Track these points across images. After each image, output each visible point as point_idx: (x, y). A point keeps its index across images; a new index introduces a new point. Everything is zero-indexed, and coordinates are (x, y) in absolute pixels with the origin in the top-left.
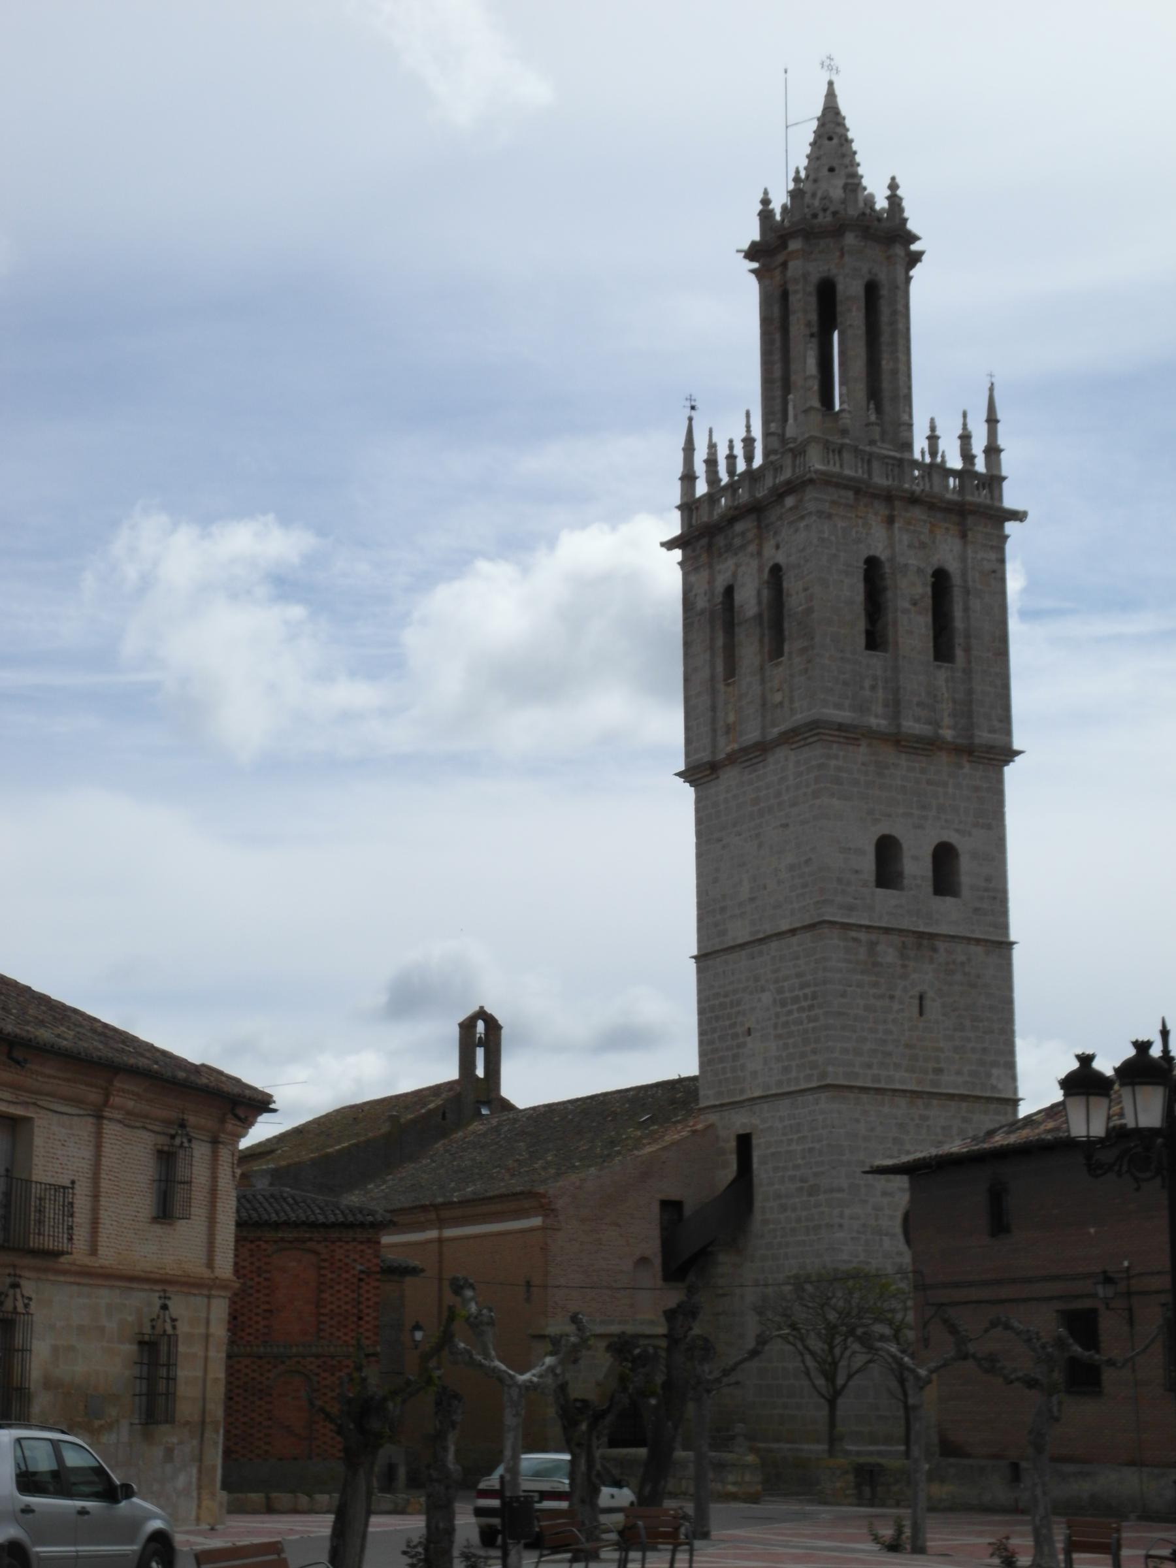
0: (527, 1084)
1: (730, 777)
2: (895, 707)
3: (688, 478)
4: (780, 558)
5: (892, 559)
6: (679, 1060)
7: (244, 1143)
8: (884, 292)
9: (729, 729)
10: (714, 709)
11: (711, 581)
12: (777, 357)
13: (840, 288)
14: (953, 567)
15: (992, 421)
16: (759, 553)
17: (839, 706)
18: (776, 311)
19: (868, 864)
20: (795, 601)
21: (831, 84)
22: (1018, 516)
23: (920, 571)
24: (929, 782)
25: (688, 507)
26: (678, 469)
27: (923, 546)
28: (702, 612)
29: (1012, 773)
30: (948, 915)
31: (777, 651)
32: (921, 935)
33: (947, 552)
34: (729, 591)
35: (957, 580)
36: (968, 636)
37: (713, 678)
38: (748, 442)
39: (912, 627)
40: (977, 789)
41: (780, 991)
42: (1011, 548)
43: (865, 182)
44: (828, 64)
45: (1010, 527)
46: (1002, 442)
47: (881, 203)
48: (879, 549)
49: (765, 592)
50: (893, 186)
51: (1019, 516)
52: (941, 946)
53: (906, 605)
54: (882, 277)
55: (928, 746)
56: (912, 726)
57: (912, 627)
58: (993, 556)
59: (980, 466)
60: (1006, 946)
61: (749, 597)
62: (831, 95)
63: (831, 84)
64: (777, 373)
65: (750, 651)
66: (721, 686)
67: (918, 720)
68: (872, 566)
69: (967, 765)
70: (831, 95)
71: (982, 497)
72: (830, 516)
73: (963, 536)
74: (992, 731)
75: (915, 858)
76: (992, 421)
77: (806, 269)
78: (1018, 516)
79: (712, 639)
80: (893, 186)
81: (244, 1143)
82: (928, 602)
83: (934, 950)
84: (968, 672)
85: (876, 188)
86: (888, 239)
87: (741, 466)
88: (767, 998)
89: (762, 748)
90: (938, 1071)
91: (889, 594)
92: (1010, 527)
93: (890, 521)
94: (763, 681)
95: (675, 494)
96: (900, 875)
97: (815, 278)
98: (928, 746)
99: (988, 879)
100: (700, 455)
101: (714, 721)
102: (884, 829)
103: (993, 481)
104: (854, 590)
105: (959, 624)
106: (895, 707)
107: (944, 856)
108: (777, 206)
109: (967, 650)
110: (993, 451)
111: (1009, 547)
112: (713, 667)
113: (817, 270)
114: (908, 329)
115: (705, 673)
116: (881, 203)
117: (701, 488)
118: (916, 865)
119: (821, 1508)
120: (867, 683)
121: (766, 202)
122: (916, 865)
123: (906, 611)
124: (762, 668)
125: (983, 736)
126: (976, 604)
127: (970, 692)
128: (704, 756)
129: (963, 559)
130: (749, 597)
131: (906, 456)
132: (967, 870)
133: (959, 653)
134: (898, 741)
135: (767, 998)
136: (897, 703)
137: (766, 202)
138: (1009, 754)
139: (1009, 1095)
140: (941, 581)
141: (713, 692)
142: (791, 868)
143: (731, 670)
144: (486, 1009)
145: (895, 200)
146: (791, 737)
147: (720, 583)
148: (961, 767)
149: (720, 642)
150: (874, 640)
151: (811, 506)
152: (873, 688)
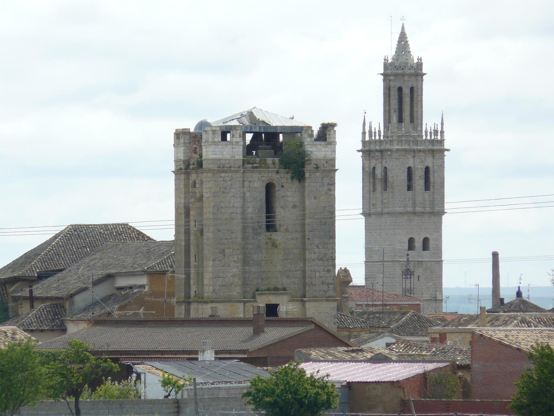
2: (414, 205)
3: (364, 133)
4: (387, 166)
5: (414, 166)
6: (364, 284)
8: (415, 89)
9: (373, 205)
10: (370, 198)
11: (370, 164)
12: (387, 104)
13: (404, 90)
14: (430, 165)
15: (442, 124)
16: (382, 163)
17: (400, 207)
18: (387, 92)
20: (390, 179)
21: (403, 24)
23: (421, 168)
24: (423, 222)
25: (364, 142)
27: (423, 161)
28: (367, 172)
30: (426, 256)
31: (385, 188)
32: (419, 261)
33: (429, 162)
34: (374, 168)
35: (431, 169)
36: (434, 183)
37: (370, 190)
38: (379, 131)
39: (419, 183)
40: (435, 222)
42: (446, 159)
43: (412, 53)
44: (403, 18)
45: (446, 153)
46: (444, 129)
48: (411, 165)
49: (383, 173)
50: (403, 85)
51: (448, 150)
52: (424, 263)
53: (418, 178)
54: (415, 85)
55: (422, 213)
56: (418, 209)
57: (419, 183)
58: (441, 161)
61: (379, 172)
62: (403, 28)
63: (403, 24)
64: (387, 109)
65: (379, 187)
66: (372, 193)
67: (420, 207)
68: (409, 169)
69: (432, 218)
70: (403, 28)
72: (399, 159)
73: (433, 157)
74: (439, 207)
75: (418, 242)
76: (442, 124)
77: (395, 84)
79: (370, 180)
82: (424, 176)
83: (422, 264)
84: (433, 193)
86: (416, 73)
87: (377, 138)
89: (382, 214)
90: (422, 294)
91: (413, 176)
92: (446, 153)
93: (414, 157)
94: (382, 196)
95: (360, 138)
96: (414, 246)
97: (397, 87)
98: (422, 213)
99: (437, 245)
100: (367, 129)
101: (370, 202)
102: (410, 236)
103: (442, 142)
104: (404, 176)
105: (431, 180)
106: (414, 205)
107: (426, 241)
109: (434, 187)
111: (445, 158)
112: (370, 187)
113: (398, 85)
114: (422, 100)
115: (367, 188)
117: (367, 138)
118: (418, 244)
119: (307, 364)
120: (407, 200)
122: (418, 244)
123: (417, 180)
124: (382, 193)
125: (437, 209)
126: (436, 175)
127: (434, 198)
129: (433, 163)
130: (379, 172)
132: (431, 244)
133: (431, 188)
134: (414, 213)
136: (415, 203)
138: (444, 213)
139: (441, 298)
140: (427, 169)
141: (370, 194)
144: (259, 116)
146: (388, 213)
147: (372, 165)
148: (431, 217)
149: (372, 181)
150: (409, 188)
151: (394, 157)
152: (409, 200)
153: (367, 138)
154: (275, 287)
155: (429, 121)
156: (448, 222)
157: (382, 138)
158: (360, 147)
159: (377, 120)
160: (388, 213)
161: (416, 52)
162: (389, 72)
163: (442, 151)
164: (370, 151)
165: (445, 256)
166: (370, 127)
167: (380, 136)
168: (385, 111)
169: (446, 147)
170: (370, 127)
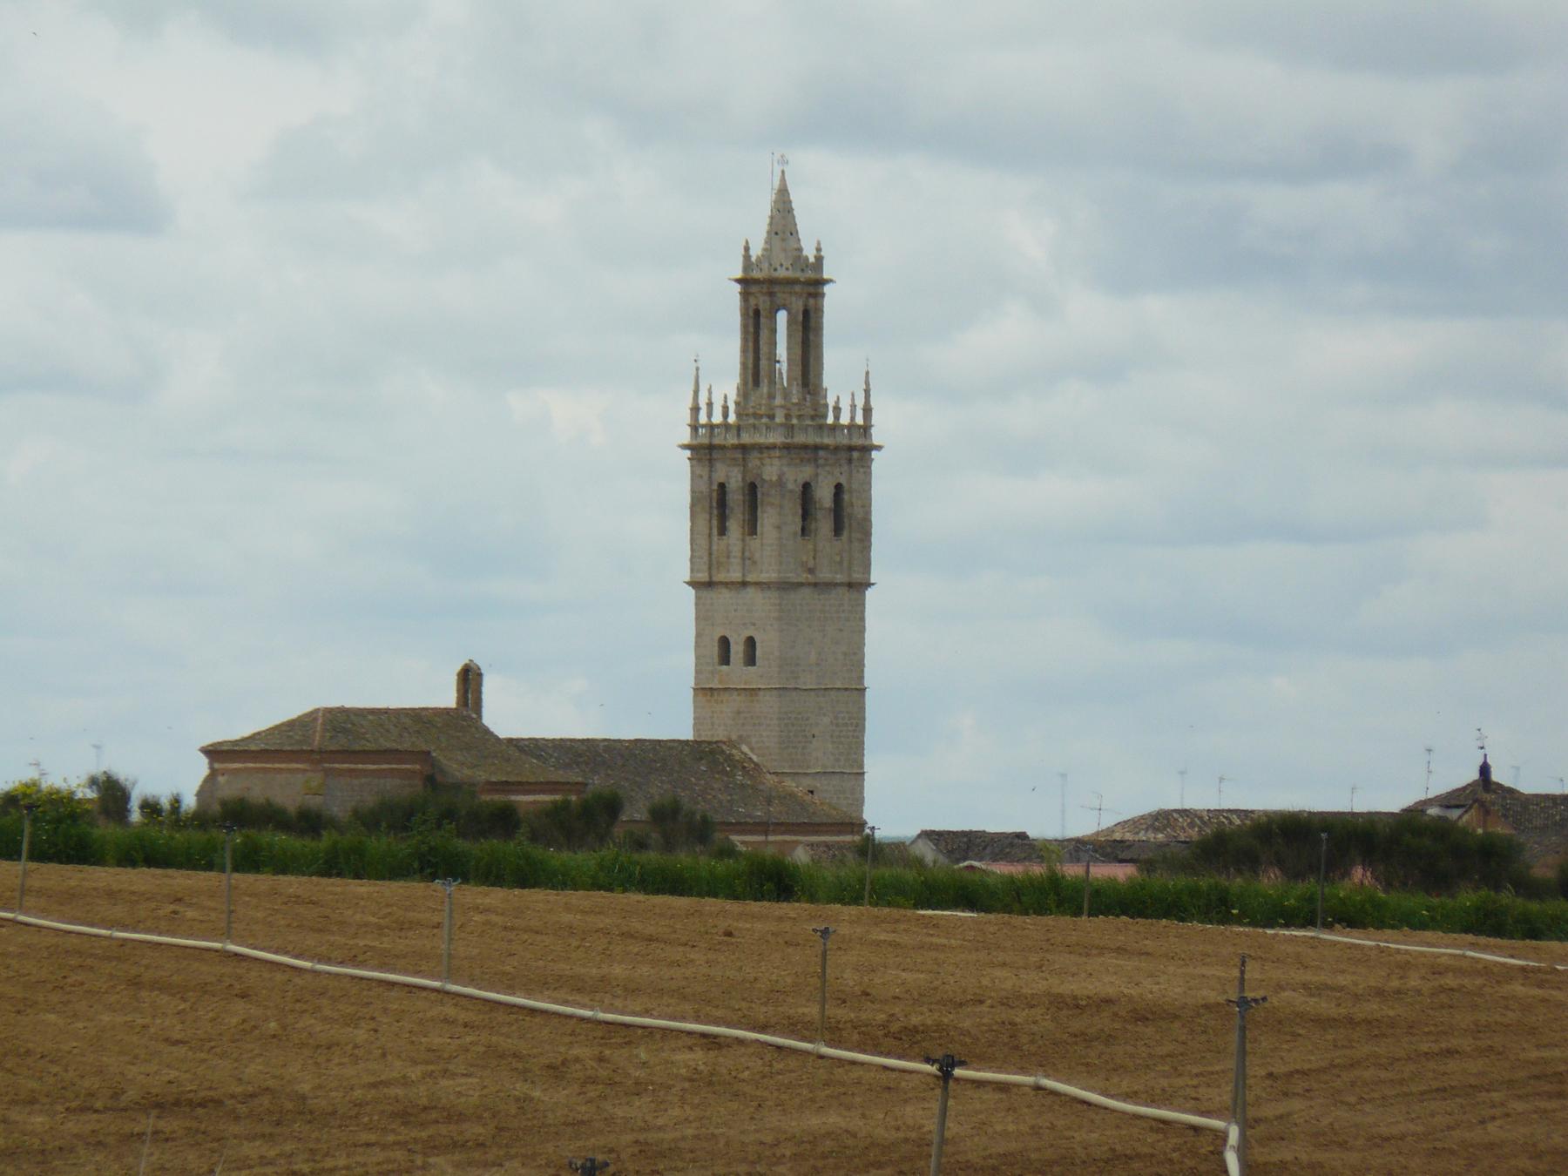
0: (985, 720)
1: (723, 597)
3: (695, 410)
15: (867, 392)
19: (715, 650)
26: (689, 403)
41: (836, 718)
46: (873, 404)
47: (812, 260)
50: (819, 250)
51: (879, 448)
59: (859, 420)
66: (715, 538)
71: (858, 441)
76: (867, 392)
80: (819, 250)
85: (809, 253)
88: (826, 720)
89: (744, 584)
95: (687, 417)
103: (866, 429)
110: (867, 411)
116: (812, 260)
118: (737, 650)
121: (747, 249)
122: (737, 650)
131: (821, 422)
132: (715, 650)
135: (826, 720)
137: (747, 249)
140: (839, 487)
142: (845, 654)
143: (723, 531)
145: (819, 259)
153: (703, 419)
157: (732, 419)
158: (685, 436)
159: (725, 387)
160: (757, 584)
162: (756, 274)
163: (867, 449)
164: (737, 404)
165: (1348, 810)
167: (726, 415)
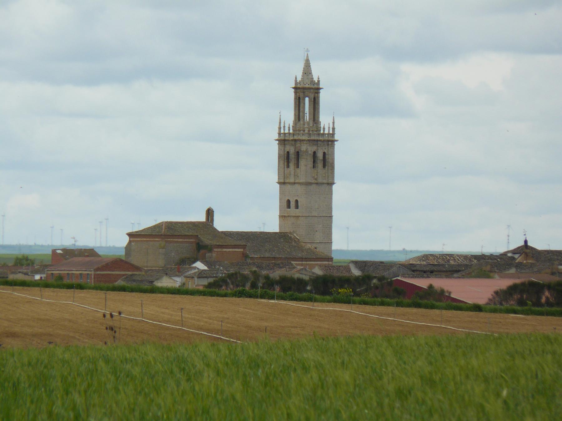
3: (280, 128)
7: (206, 268)
15: (333, 123)
22: (337, 141)
25: (280, 134)
26: (278, 126)
29: (334, 187)
47: (316, 81)
59: (331, 132)
60: (331, 217)
61: (320, 155)
66: (286, 168)
76: (333, 123)
78: (337, 141)
81: (206, 268)
85: (316, 79)
88: (321, 226)
89: (295, 183)
108: (299, 79)
110: (334, 129)
118: (293, 204)
121: (296, 78)
122: (293, 204)
128: (282, 181)
135: (321, 226)
140: (324, 153)
143: (288, 167)
145: (319, 81)
153: (282, 131)
154: (5, 264)
155: (325, 121)
156: (340, 192)
157: (291, 131)
161: (316, 74)
162: (299, 86)
163: (333, 141)
166: (284, 123)
167: (289, 130)
168: (447, 257)
169: (336, 138)
170: (284, 123)
